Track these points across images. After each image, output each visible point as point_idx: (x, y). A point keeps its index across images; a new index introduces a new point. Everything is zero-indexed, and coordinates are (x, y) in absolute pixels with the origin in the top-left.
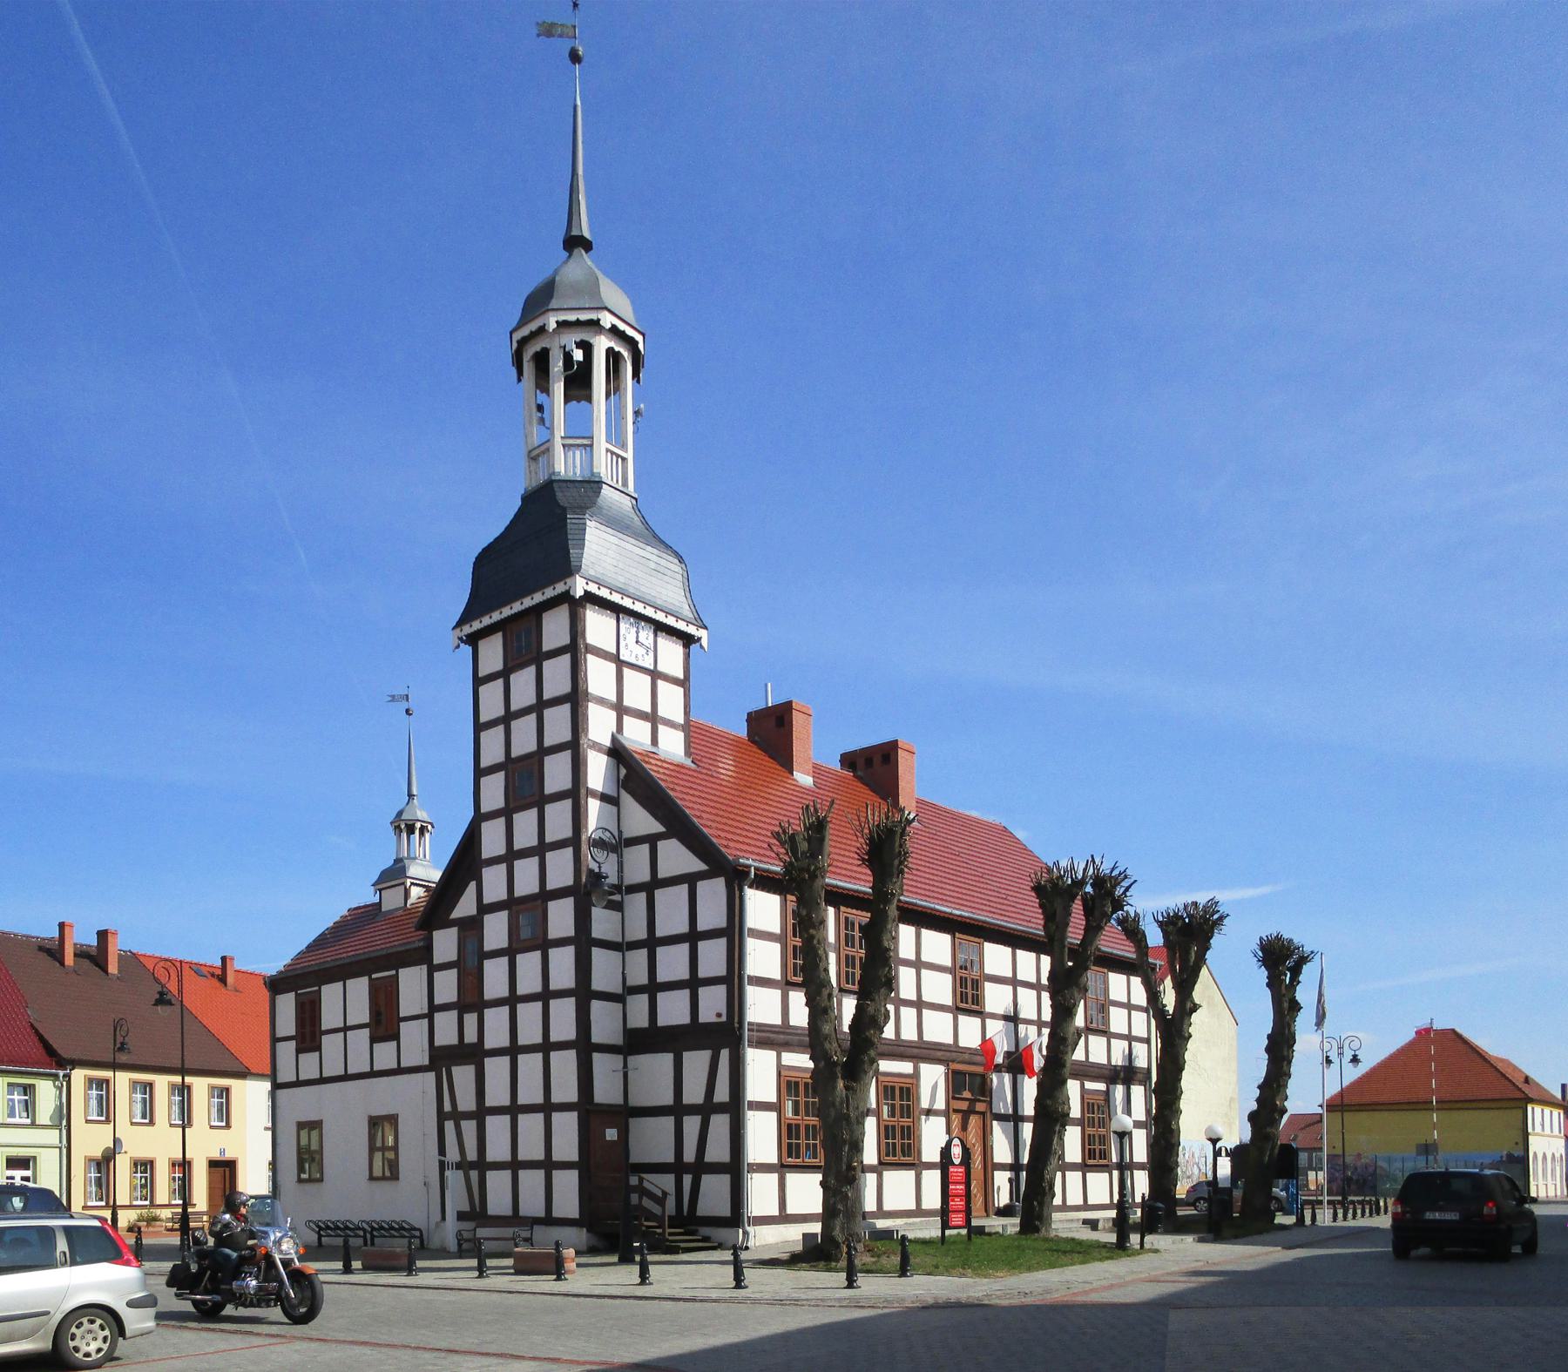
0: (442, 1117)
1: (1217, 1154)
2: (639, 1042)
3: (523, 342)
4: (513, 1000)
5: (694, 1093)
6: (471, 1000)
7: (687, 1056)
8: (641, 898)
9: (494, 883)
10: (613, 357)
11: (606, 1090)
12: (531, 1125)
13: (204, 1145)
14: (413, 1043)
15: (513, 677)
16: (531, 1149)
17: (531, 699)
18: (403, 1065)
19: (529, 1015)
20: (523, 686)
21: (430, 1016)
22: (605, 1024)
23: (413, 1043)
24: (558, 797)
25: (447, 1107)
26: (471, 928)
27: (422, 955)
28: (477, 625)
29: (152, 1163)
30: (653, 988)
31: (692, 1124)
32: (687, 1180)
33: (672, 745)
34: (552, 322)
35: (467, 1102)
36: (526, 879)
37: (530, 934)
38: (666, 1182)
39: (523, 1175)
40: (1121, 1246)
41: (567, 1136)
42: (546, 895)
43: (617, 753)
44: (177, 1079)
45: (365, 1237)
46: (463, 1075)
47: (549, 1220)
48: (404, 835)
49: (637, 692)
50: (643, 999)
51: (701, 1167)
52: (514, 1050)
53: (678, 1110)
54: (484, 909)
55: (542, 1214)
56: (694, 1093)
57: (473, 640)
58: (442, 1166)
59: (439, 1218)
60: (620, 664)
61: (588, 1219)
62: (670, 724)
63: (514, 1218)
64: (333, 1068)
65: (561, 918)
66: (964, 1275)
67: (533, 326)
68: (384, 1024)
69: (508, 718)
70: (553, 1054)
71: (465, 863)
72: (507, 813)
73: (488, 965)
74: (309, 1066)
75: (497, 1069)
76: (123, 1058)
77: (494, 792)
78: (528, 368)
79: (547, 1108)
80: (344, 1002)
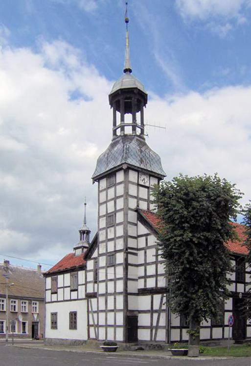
2: (144, 292)
5: (156, 307)
8: (143, 252)
9: (102, 249)
10: (139, 101)
14: (82, 293)
15: (108, 203)
20: (111, 192)
21: (86, 284)
24: (120, 224)
25: (90, 310)
30: (146, 277)
31: (155, 315)
36: (111, 248)
37: (112, 264)
41: (120, 319)
42: (116, 251)
46: (94, 300)
50: (143, 280)
53: (152, 311)
54: (100, 255)
56: (156, 307)
64: (61, 298)
65: (120, 258)
74: (54, 297)
77: (103, 223)
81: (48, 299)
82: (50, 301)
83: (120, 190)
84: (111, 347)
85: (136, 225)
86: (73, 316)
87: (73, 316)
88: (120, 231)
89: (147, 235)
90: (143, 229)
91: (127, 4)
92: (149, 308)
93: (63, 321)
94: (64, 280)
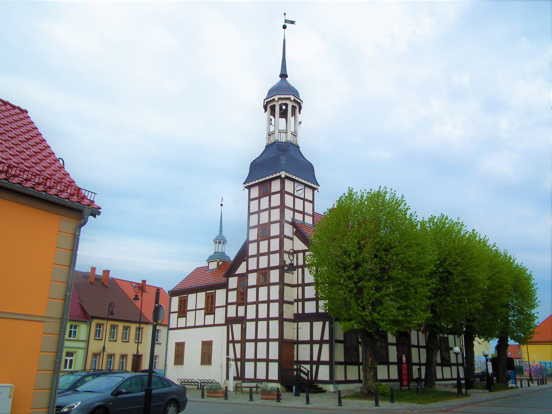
0: (228, 342)
1: (487, 360)
2: (299, 318)
3: (268, 103)
4: (257, 303)
6: (242, 300)
7: (315, 324)
10: (294, 108)
11: (289, 334)
12: (262, 346)
13: (130, 349)
14: (220, 316)
16: (262, 354)
17: (267, 206)
18: (215, 323)
19: (263, 308)
20: (265, 202)
21: (226, 306)
22: (290, 311)
23: (220, 316)
25: (231, 339)
26: (243, 277)
27: (225, 286)
28: (251, 183)
29: (114, 355)
31: (316, 347)
32: (314, 367)
33: (309, 220)
34: (276, 98)
35: (238, 337)
36: (263, 263)
38: (308, 367)
39: (258, 364)
40: (459, 394)
41: (274, 351)
42: (270, 268)
43: (293, 223)
44: (138, 325)
45: (198, 385)
46: (237, 328)
47: (267, 380)
48: (217, 244)
49: (299, 205)
51: (319, 363)
52: (257, 320)
53: (311, 342)
54: (249, 272)
55: (265, 378)
56: (317, 336)
57: (249, 188)
58: (228, 360)
59: (225, 378)
60: (295, 197)
61: (282, 379)
62: (309, 215)
63: (255, 380)
64: (190, 323)
65: (274, 276)
66: (414, 403)
67: (271, 99)
68: (210, 309)
69: (259, 212)
70: (270, 322)
71: (243, 255)
72: (258, 241)
73: (249, 290)
74: (182, 322)
75: (250, 326)
76: (110, 317)
77: (254, 235)
78: (268, 109)
79: (268, 340)
80: (197, 300)
81: (173, 325)
82: (343, 379)
83: (276, 200)
84: (255, 389)
85: (292, 239)
86: (207, 346)
87: (207, 346)
88: (275, 244)
89: (304, 251)
90: (299, 245)
91: (285, 14)
92: (308, 338)
93: (193, 353)
94: (197, 300)
